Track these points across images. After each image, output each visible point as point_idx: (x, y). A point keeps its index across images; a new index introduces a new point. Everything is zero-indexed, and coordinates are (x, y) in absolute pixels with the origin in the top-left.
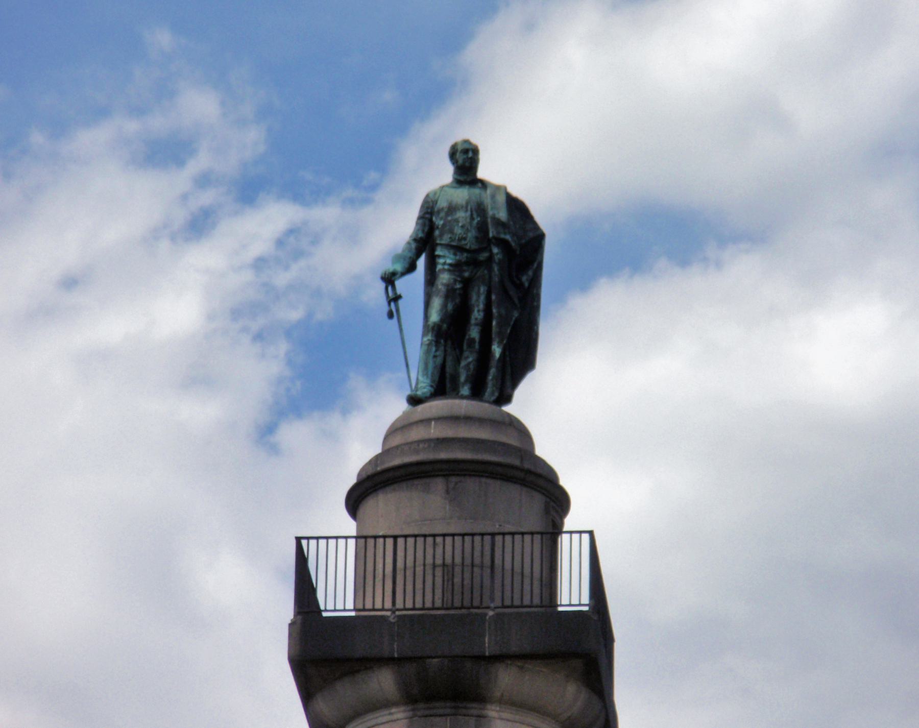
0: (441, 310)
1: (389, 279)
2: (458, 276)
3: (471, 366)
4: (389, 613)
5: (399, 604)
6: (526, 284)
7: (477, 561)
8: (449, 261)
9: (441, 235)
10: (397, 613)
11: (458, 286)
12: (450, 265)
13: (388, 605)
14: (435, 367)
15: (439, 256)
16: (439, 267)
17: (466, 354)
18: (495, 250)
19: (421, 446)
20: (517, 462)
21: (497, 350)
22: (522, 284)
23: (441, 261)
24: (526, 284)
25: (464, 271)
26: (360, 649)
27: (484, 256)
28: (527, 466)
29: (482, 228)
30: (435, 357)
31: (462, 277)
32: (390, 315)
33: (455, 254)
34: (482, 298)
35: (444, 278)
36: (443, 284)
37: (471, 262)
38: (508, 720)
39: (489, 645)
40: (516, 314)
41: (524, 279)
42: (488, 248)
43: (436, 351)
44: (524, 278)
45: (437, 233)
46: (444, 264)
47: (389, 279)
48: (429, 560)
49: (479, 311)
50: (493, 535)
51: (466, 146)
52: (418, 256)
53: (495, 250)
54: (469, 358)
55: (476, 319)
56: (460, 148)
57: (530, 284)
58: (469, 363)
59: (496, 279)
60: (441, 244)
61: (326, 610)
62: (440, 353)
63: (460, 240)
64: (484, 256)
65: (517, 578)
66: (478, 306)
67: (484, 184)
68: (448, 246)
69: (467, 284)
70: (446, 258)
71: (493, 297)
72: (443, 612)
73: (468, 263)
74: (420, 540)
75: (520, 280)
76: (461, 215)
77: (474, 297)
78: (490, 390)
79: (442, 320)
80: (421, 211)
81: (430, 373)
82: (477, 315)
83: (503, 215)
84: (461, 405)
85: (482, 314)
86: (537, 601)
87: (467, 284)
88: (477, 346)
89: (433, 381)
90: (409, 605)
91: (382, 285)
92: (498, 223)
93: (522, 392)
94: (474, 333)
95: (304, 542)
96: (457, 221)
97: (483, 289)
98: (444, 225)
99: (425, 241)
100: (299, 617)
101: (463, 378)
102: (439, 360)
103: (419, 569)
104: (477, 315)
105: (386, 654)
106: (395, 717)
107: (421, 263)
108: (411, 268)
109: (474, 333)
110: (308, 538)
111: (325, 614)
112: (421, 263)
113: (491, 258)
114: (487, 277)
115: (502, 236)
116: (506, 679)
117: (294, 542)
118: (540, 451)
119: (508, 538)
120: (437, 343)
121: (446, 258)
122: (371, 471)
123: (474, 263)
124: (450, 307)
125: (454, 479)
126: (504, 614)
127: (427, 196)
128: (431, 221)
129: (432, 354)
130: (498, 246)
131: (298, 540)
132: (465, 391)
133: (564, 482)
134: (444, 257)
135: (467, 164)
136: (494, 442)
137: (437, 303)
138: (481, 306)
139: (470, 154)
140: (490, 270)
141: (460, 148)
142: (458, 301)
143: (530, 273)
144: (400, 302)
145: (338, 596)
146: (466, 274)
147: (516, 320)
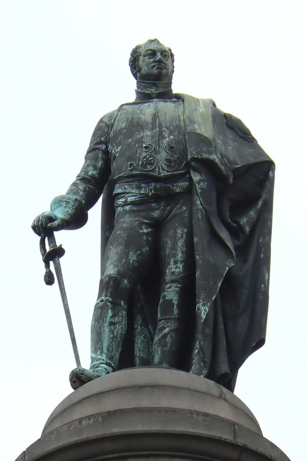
0: (119, 260)
1: (45, 228)
2: (145, 217)
3: (168, 339)
12: (132, 203)
14: (113, 338)
16: (119, 209)
17: (161, 324)
19: (84, 423)
20: (228, 437)
21: (203, 310)
22: (241, 229)
23: (121, 201)
25: (153, 209)
27: (179, 187)
28: (241, 441)
30: (111, 324)
31: (151, 218)
32: (49, 280)
33: (139, 188)
35: (125, 221)
36: (122, 229)
37: (163, 193)
42: (186, 176)
43: (113, 316)
44: (243, 221)
46: (126, 204)
47: (45, 228)
49: (176, 262)
51: (153, 46)
52: (91, 203)
53: (196, 177)
55: (173, 273)
56: (142, 51)
58: (165, 336)
60: (120, 179)
62: (122, 318)
64: (179, 187)
66: (175, 255)
67: (179, 98)
68: (131, 178)
69: (158, 227)
70: (129, 194)
71: (195, 240)
73: (157, 198)
75: (238, 223)
77: (169, 243)
80: (91, 142)
81: (105, 345)
82: (174, 268)
85: (181, 266)
87: (158, 227)
88: (176, 311)
91: (37, 238)
94: (171, 293)
99: (98, 181)
102: (120, 329)
104: (174, 268)
107: (95, 213)
108: (77, 220)
109: (171, 293)
112: (95, 213)
113: (190, 191)
114: (186, 215)
118: (267, 434)
121: (129, 194)
123: (165, 197)
124: (133, 257)
127: (101, 121)
128: (106, 153)
135: (155, 71)
136: (191, 412)
138: (180, 256)
139: (159, 56)
140: (191, 205)
141: (142, 51)
142: (146, 249)
143: (252, 213)
144: (62, 260)
146: (156, 214)
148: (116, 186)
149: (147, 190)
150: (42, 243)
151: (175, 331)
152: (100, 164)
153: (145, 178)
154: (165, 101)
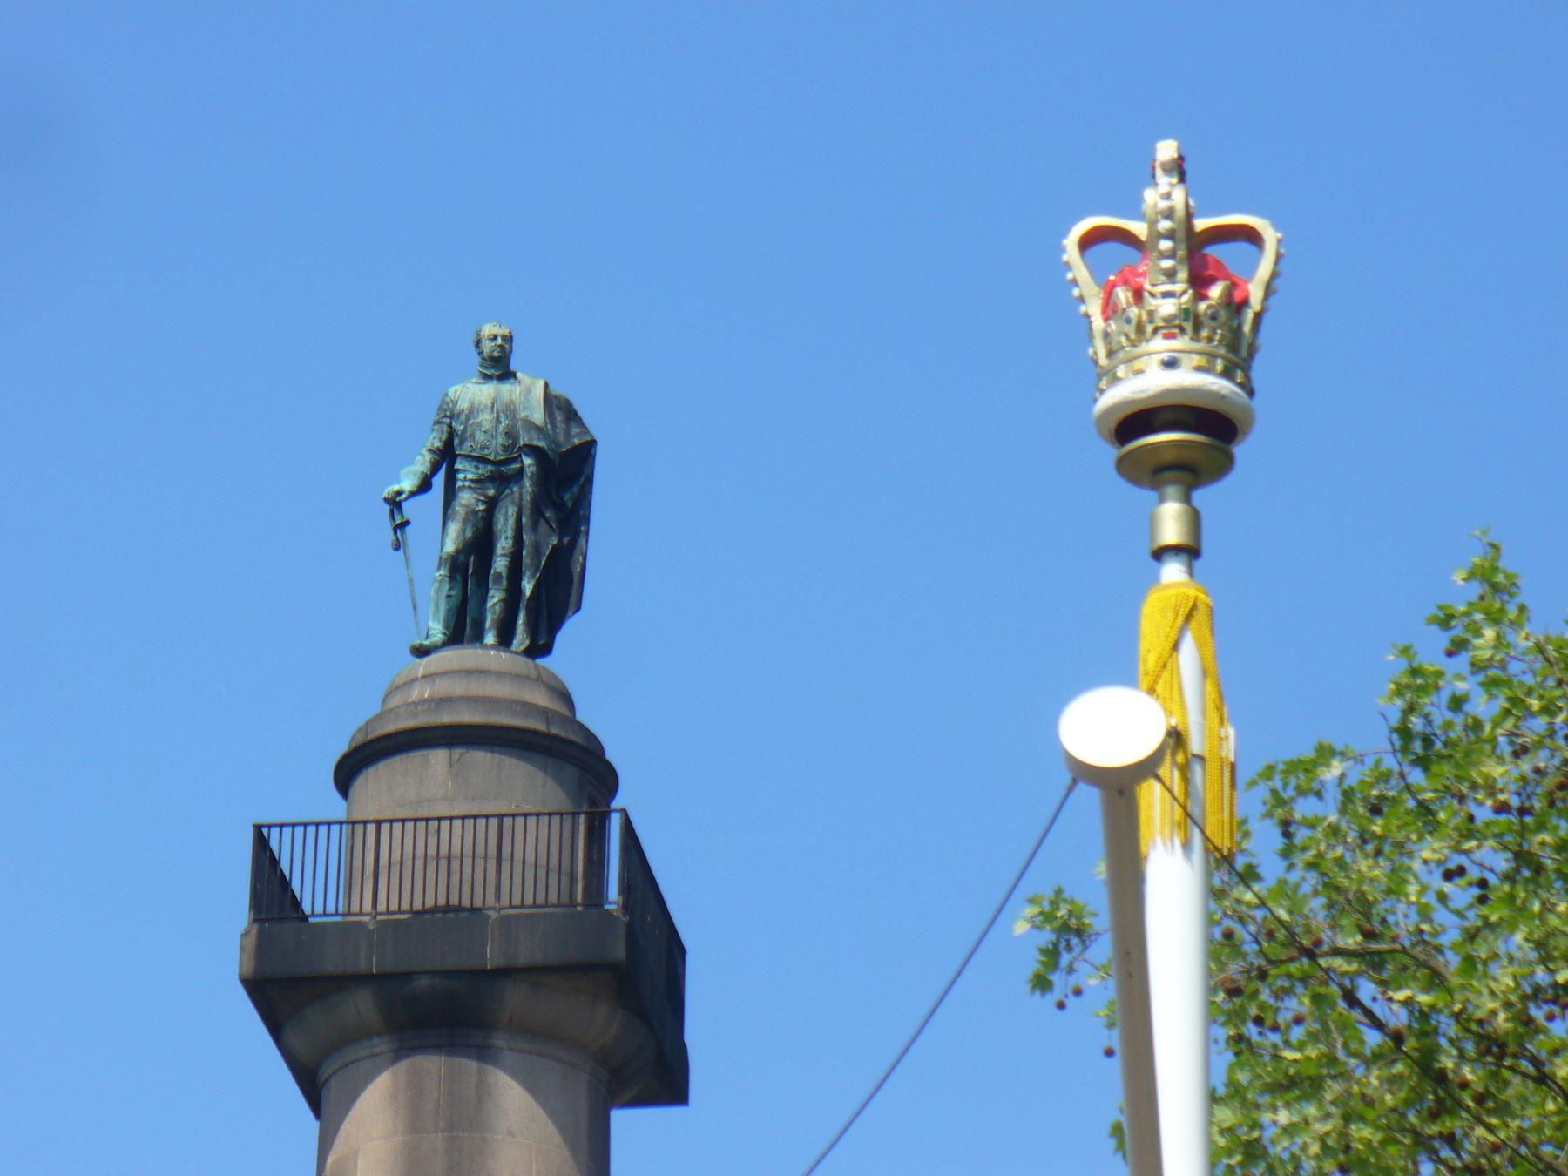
1: (395, 503)
3: (497, 608)
4: (367, 919)
5: (381, 907)
6: (570, 504)
7: (456, 850)
8: (470, 476)
9: (462, 443)
10: (503, 912)
11: (481, 507)
13: (367, 907)
14: (448, 611)
15: (458, 471)
16: (459, 484)
17: (492, 592)
18: (527, 461)
21: (528, 587)
22: (564, 504)
23: (461, 476)
24: (570, 504)
26: (331, 962)
29: (511, 434)
32: (397, 548)
34: (511, 522)
35: (466, 498)
36: (462, 505)
38: (519, 1051)
39: (492, 957)
40: (554, 541)
41: (567, 497)
44: (567, 497)
45: (456, 441)
46: (465, 479)
48: (432, 852)
50: (501, 817)
54: (495, 597)
57: (575, 505)
59: (527, 498)
61: (313, 915)
63: (483, 448)
65: (542, 873)
69: (492, 504)
72: (339, 919)
73: (491, 478)
74: (421, 825)
76: (486, 418)
78: (521, 639)
79: (458, 552)
83: (538, 416)
84: (485, 654)
85: (511, 541)
86: (553, 898)
87: (492, 504)
88: (504, 582)
89: (446, 627)
90: (394, 906)
91: (387, 508)
92: (530, 425)
93: (566, 637)
94: (500, 564)
95: (265, 831)
96: (479, 425)
97: (512, 510)
98: (465, 430)
100: (256, 926)
101: (488, 624)
103: (408, 863)
104: (503, 544)
105: (362, 967)
106: (377, 1050)
107: (439, 480)
110: (270, 826)
111: (312, 920)
113: (521, 471)
115: (536, 443)
116: (514, 997)
117: (251, 830)
118: (581, 716)
119: (520, 821)
120: (452, 578)
121: (467, 472)
122: (360, 739)
124: (469, 534)
125: (457, 752)
126: (509, 917)
129: (445, 593)
130: (528, 455)
131: (258, 828)
132: (490, 639)
133: (611, 756)
134: (464, 471)
137: (454, 528)
138: (510, 533)
143: (575, 490)
145: (319, 893)
146: (491, 492)
147: (554, 548)
148: (376, 1041)
149: (485, 470)
150: (392, 512)
151: (503, 601)
152: (445, 437)
153: (483, 460)
154: (470, 665)
